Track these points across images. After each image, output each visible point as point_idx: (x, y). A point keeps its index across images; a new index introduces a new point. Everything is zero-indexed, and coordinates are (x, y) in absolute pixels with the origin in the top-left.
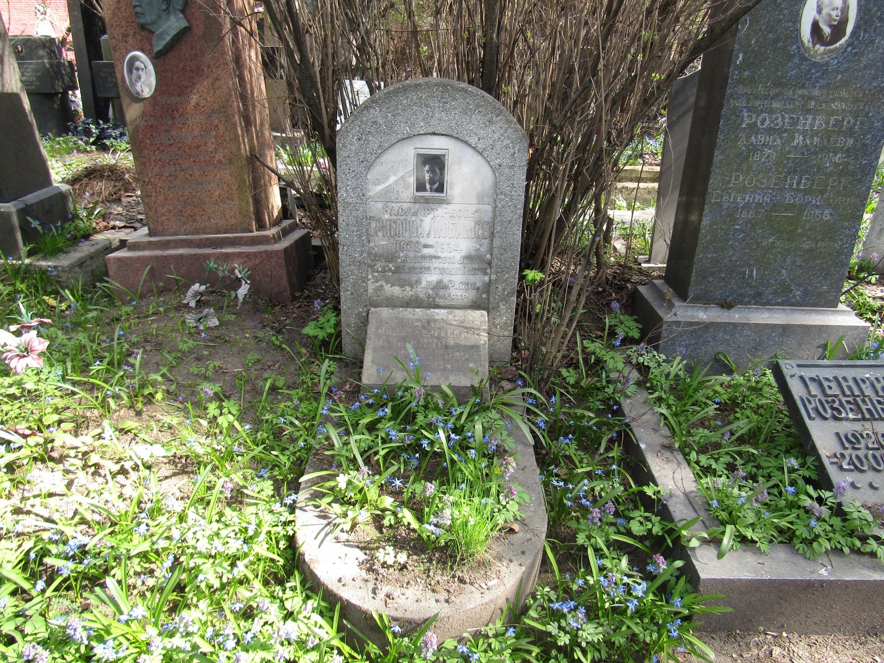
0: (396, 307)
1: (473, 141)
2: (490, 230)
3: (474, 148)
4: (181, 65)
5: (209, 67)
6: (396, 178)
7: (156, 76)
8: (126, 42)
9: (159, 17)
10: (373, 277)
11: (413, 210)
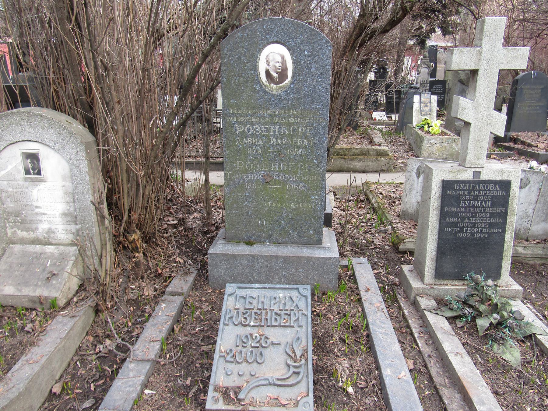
0: (26, 244)
1: (52, 145)
2: (73, 197)
3: (54, 149)
6: (12, 167)
10: (10, 226)
11: (25, 186)
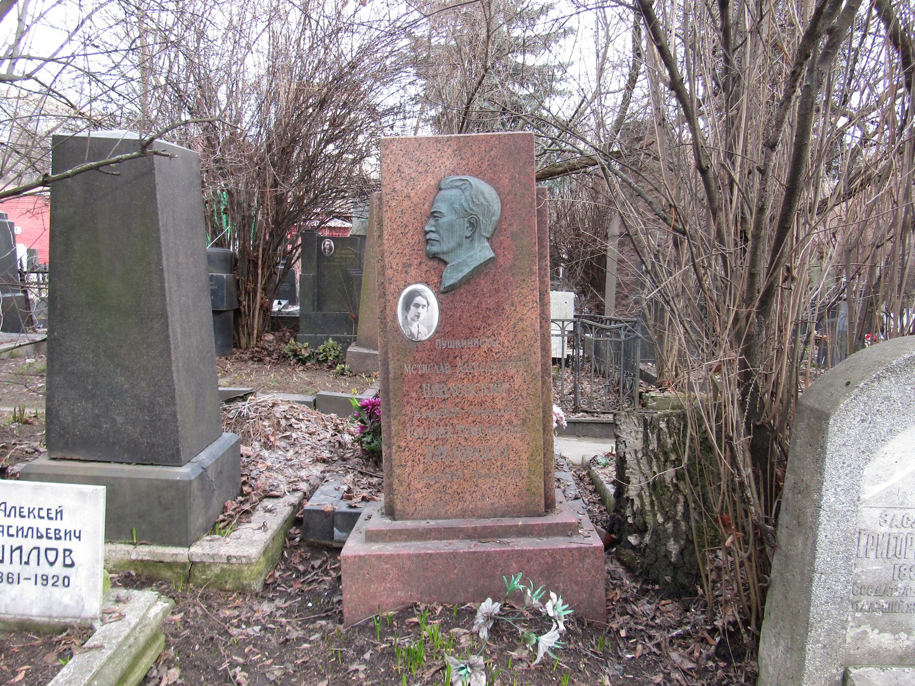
4: (475, 302)
5: (512, 305)
7: (440, 314)
8: (406, 272)
9: (460, 245)
